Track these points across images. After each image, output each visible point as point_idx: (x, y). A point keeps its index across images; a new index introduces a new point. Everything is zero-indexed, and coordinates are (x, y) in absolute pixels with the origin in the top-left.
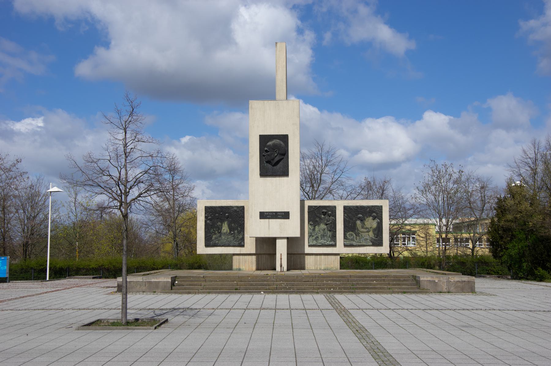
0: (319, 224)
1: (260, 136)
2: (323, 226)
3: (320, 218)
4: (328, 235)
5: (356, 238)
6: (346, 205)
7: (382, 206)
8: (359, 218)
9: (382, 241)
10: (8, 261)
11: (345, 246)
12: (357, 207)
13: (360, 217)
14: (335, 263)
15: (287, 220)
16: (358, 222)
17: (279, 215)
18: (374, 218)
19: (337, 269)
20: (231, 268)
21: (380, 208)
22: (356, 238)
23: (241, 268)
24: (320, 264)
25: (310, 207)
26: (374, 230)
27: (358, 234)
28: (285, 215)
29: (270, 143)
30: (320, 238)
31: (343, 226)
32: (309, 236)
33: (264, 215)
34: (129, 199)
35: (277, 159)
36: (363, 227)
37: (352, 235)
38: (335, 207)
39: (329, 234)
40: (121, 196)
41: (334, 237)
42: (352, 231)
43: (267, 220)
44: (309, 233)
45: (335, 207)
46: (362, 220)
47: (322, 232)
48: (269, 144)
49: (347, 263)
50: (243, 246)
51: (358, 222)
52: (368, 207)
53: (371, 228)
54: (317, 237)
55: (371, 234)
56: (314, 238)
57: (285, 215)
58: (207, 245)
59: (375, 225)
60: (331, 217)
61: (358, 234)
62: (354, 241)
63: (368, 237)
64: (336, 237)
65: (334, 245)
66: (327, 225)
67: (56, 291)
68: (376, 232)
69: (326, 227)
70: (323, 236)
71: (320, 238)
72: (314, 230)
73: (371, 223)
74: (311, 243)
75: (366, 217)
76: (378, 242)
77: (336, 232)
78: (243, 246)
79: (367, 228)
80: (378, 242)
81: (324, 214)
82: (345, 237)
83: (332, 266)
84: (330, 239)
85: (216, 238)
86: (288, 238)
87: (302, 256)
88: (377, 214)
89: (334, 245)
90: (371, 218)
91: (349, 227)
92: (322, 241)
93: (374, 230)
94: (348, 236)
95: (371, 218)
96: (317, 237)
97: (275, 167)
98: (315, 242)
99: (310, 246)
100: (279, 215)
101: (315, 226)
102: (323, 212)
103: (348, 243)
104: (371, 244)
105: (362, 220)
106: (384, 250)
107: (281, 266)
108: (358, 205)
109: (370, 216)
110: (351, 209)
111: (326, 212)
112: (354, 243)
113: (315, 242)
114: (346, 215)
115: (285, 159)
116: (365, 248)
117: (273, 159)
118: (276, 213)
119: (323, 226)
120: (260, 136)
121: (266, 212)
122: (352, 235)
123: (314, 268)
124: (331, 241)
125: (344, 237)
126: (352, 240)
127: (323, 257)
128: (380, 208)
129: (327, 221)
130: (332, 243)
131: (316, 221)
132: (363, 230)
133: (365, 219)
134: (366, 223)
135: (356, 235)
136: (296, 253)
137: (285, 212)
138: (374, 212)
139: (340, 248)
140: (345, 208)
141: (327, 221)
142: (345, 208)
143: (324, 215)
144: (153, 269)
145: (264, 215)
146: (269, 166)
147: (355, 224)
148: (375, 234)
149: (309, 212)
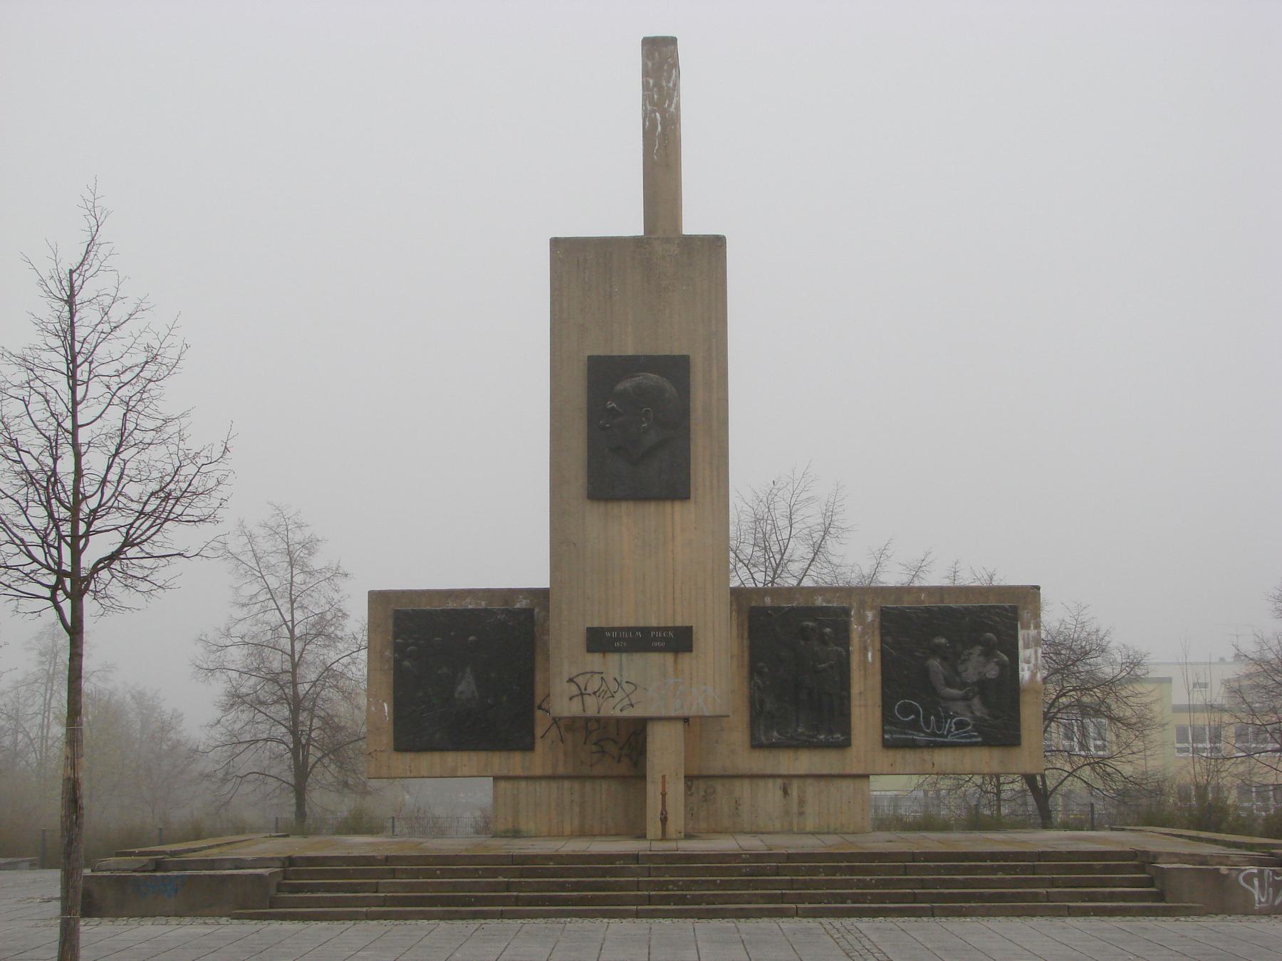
1: (555, 243)
8: (935, 651)
23: (523, 827)
28: (679, 641)
29: (625, 385)
33: (600, 640)
34: (88, 560)
36: (949, 684)
40: (59, 549)
48: (622, 386)
51: (935, 663)
57: (679, 641)
79: (963, 685)
97: (594, 661)
100: (655, 639)
107: (664, 820)
112: (920, 737)
118: (646, 630)
120: (555, 243)
121: (612, 629)
125: (884, 715)
126: (914, 725)
137: (676, 630)
145: (600, 640)
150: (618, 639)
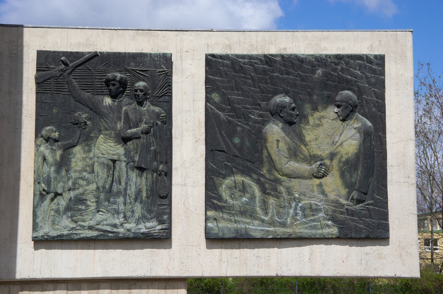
0: (88, 140)
2: (106, 147)
3: (96, 111)
4: (132, 190)
5: (265, 204)
6: (218, 51)
7: (380, 60)
8: (277, 113)
9: (385, 216)
11: (214, 240)
12: (268, 60)
13: (282, 107)
15: (39, 49)
16: (274, 131)
18: (347, 113)
22: (265, 204)
25: (45, 58)
26: (348, 167)
27: (270, 188)
30: (92, 204)
31: (202, 148)
36: (294, 154)
37: (244, 189)
38: (167, 60)
39: (137, 182)
41: (160, 199)
42: (246, 172)
44: (37, 182)
45: (167, 60)
46: (292, 121)
47: (101, 172)
51: (274, 131)
52: (320, 61)
53: (332, 156)
54: (81, 200)
55: (333, 184)
56: (63, 202)
59: (349, 140)
60: (148, 107)
61: (270, 188)
62: (253, 216)
63: (316, 200)
64: (167, 196)
65: (163, 239)
66: (125, 140)
69: (120, 150)
70: (108, 193)
71: (92, 204)
72: (63, 164)
73: (332, 134)
74: (47, 229)
75: (307, 108)
77: (168, 174)
79: (313, 158)
81: (118, 90)
82: (213, 200)
84: (138, 209)
88: (360, 93)
89: (163, 239)
91: (232, 150)
92: (104, 220)
93: (348, 167)
94: (225, 195)
96: (81, 200)
98: (65, 225)
99: (40, 242)
101: (67, 149)
102: (108, 82)
103: (225, 226)
104: (334, 231)
105: (292, 121)
108: (273, 50)
109: (329, 101)
110: (242, 70)
111: (123, 84)
112: (255, 228)
116: (306, 250)
119: (106, 147)
122: (244, 189)
124: (143, 218)
125: (208, 198)
126: (247, 212)
129: (129, 124)
130: (152, 226)
131: (77, 123)
132: (294, 166)
133: (303, 117)
134: (309, 136)
135: (264, 191)
137: (386, 228)
138: (348, 85)
140: (213, 63)
141: (129, 124)
142: (213, 63)
143: (114, 97)
147: (259, 139)
148: (350, 186)
149: (40, 83)
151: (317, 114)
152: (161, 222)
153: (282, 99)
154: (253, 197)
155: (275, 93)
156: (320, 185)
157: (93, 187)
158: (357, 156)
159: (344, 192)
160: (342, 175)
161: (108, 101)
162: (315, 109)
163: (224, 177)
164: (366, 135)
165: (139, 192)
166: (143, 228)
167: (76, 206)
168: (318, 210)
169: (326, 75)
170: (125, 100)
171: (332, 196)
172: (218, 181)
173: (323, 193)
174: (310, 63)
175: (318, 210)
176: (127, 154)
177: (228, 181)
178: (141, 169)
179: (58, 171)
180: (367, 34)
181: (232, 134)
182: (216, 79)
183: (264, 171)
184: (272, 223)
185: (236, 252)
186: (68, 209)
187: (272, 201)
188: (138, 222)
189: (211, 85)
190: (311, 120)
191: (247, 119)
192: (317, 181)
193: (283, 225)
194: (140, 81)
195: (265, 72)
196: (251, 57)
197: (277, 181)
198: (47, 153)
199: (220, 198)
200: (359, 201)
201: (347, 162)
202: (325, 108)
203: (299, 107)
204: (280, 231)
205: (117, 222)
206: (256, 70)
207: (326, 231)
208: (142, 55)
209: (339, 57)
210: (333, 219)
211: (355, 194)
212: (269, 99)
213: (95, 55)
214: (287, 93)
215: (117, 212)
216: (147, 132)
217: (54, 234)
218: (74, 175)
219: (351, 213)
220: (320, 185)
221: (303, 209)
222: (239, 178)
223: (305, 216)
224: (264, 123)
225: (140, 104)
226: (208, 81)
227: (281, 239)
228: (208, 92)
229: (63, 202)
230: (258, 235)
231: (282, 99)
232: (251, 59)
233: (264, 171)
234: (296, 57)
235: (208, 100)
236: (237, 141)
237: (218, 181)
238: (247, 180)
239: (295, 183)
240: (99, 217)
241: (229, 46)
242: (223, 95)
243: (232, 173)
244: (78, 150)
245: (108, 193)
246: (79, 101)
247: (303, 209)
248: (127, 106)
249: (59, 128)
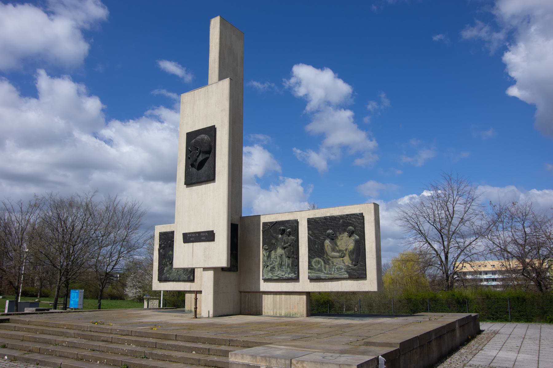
0: (275, 249)
2: (280, 251)
3: (277, 239)
5: (325, 267)
6: (311, 217)
8: (328, 236)
9: (365, 270)
10: (83, 294)
11: (311, 279)
12: (325, 218)
13: (329, 234)
14: (299, 305)
16: (327, 242)
17: (203, 236)
18: (351, 234)
19: (302, 316)
20: (259, 313)
21: (360, 218)
22: (325, 267)
24: (280, 308)
25: (265, 224)
28: (209, 236)
30: (277, 268)
32: (264, 267)
33: (189, 238)
35: (200, 158)
36: (333, 250)
37: (319, 262)
39: (287, 261)
41: (295, 266)
42: (319, 257)
43: (192, 244)
46: (333, 239)
49: (320, 305)
50: (193, 281)
51: (327, 242)
52: (342, 217)
53: (346, 250)
54: (274, 268)
55: (347, 259)
56: (269, 268)
57: (209, 236)
58: (160, 280)
61: (326, 262)
62: (321, 271)
63: (342, 266)
64: (298, 265)
65: (296, 279)
66: (284, 248)
67: (17, 314)
68: (354, 256)
69: (283, 252)
71: (277, 268)
72: (269, 256)
73: (346, 242)
75: (338, 234)
76: (358, 273)
78: (193, 281)
79: (339, 251)
80: (358, 273)
81: (283, 232)
82: (310, 267)
83: (295, 311)
84: (289, 269)
85: (167, 271)
86: (215, 269)
87: (258, 294)
88: (355, 227)
89: (296, 279)
90: (346, 234)
91: (316, 250)
92: (279, 273)
93: (351, 253)
94: (313, 265)
95: (346, 234)
96: (274, 268)
98: (270, 275)
99: (266, 280)
100: (203, 236)
101: (270, 252)
103: (314, 275)
104: (347, 276)
106: (369, 285)
108: (328, 215)
109: (345, 231)
110: (317, 222)
112: (322, 275)
113: (270, 274)
114: (310, 232)
115: (210, 159)
116: (340, 282)
117: (196, 160)
119: (280, 251)
122: (319, 262)
123: (272, 314)
126: (320, 270)
127: (283, 296)
128: (360, 218)
129: (285, 243)
130: (292, 275)
133: (337, 237)
135: (325, 263)
136: (249, 290)
138: (351, 224)
139: (305, 284)
140: (310, 221)
141: (285, 243)
142: (310, 221)
144: (45, 297)
145: (189, 238)
146: (194, 170)
148: (352, 260)
150: (191, 237)
151: (341, 236)
152: (295, 274)
153: (330, 231)
154: (321, 265)
155: (328, 229)
156: (343, 260)
157: (277, 263)
158: (354, 249)
159: (350, 262)
160: (349, 256)
161: (280, 236)
162: (340, 234)
163: (313, 259)
164: (356, 241)
165: (288, 265)
166: (290, 276)
167: (272, 270)
168: (342, 269)
169: (343, 222)
170: (285, 235)
171: (347, 264)
172: (311, 260)
173: (344, 263)
174: (338, 218)
175: (342, 269)
176: (285, 253)
177: (314, 260)
178: (289, 257)
179: (267, 259)
180: (358, 206)
181: (315, 244)
182: (163, 299)
183: (325, 256)
184: (327, 274)
185: (318, 283)
186: (271, 270)
187: (327, 266)
188: (289, 274)
189: (309, 229)
190: (339, 238)
191: (319, 239)
192: (342, 259)
193: (331, 274)
194: (292, 227)
195: (324, 222)
196: (320, 218)
197: (329, 259)
198: (265, 253)
199: (312, 266)
200: (355, 265)
201: (350, 252)
202: (343, 233)
203: (335, 234)
204: (330, 276)
205: (283, 274)
206: (322, 222)
207: (345, 276)
208: (289, 221)
209: (347, 215)
210: (347, 272)
211: (354, 263)
212: (326, 232)
213: (276, 222)
214: (331, 229)
215: (283, 271)
216: (290, 245)
217: (267, 278)
218: (272, 260)
219: (353, 269)
220: (343, 260)
221: (337, 269)
222: (317, 259)
223: (338, 271)
224: (325, 240)
225: (289, 236)
226: (308, 227)
227: (330, 279)
228: (308, 231)
229: (269, 268)
230: (323, 278)
231: (330, 231)
232: (320, 218)
233: (325, 256)
234: (334, 216)
235: (308, 233)
236: (316, 246)
237: (311, 260)
238: (320, 259)
239: (334, 260)
240: (278, 273)
241: (315, 215)
242: (312, 231)
243: (315, 258)
244: (273, 252)
245: (281, 265)
246: (273, 237)
247: (337, 269)
248: (285, 237)
249: (268, 245)
